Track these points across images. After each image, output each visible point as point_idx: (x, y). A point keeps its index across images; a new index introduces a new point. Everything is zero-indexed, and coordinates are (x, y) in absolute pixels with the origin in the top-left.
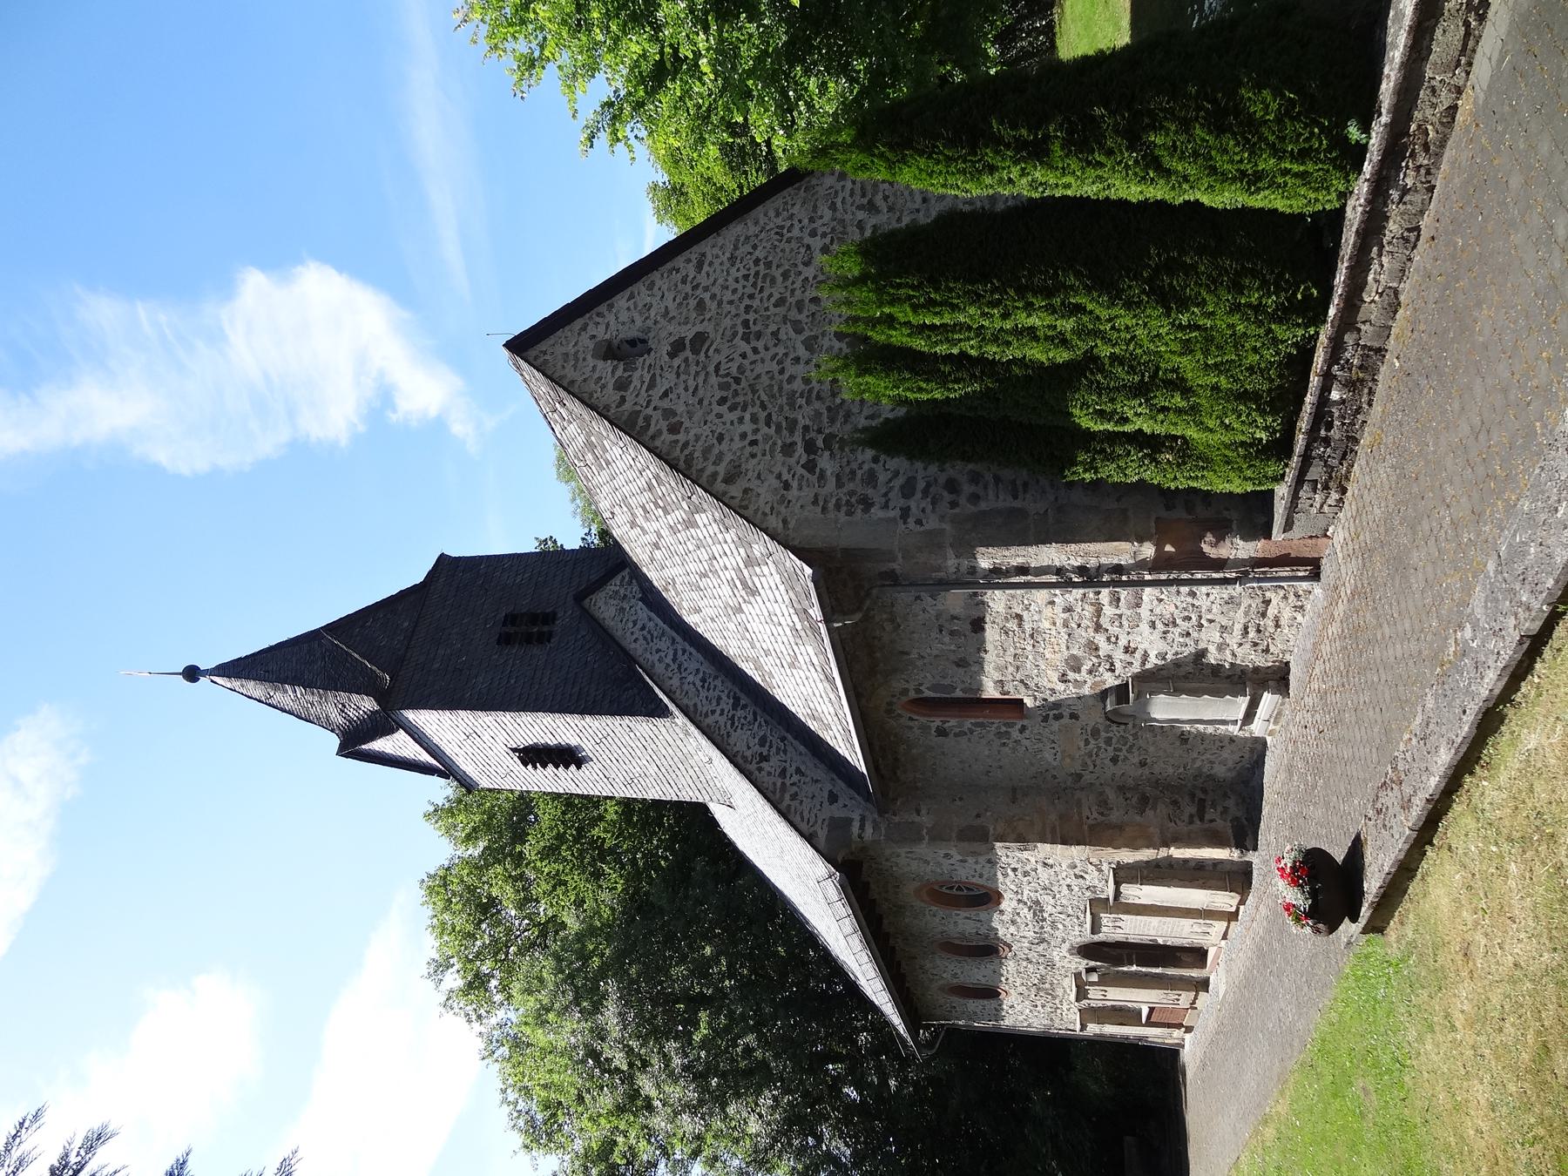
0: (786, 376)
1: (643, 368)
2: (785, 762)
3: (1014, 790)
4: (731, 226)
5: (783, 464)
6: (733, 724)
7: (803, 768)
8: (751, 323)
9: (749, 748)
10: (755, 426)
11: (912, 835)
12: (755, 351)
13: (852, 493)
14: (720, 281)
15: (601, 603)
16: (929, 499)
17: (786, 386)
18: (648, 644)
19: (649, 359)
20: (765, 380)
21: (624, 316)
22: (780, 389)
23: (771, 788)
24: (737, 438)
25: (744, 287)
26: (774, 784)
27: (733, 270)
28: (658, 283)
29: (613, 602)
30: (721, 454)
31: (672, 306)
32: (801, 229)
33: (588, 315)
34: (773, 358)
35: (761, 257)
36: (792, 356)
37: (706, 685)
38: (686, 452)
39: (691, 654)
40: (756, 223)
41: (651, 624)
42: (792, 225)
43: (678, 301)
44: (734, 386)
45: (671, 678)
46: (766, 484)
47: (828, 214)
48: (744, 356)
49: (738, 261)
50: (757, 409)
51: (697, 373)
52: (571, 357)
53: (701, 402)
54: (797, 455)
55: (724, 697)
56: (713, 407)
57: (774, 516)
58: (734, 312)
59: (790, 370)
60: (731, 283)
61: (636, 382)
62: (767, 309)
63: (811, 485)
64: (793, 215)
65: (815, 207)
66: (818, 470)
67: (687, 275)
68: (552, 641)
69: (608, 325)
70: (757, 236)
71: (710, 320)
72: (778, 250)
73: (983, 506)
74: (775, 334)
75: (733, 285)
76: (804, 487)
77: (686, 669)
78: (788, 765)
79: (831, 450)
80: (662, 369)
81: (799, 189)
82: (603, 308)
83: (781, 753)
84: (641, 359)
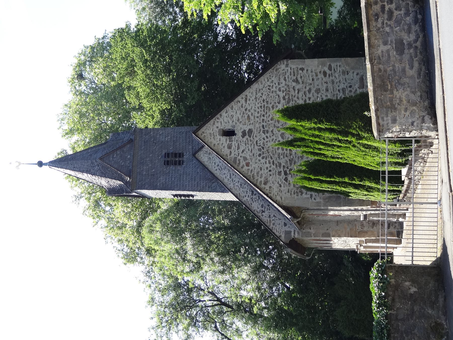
1: (235, 141)
3: (337, 222)
6: (252, 200)
7: (276, 215)
9: (258, 208)
11: (309, 235)
12: (267, 137)
14: (253, 108)
15: (202, 156)
22: (276, 152)
23: (266, 221)
24: (265, 169)
25: (261, 111)
26: (267, 220)
27: (257, 103)
28: (234, 107)
29: (205, 155)
30: (262, 174)
31: (240, 117)
32: (276, 87)
33: (214, 118)
36: (278, 140)
37: (242, 186)
38: (252, 173)
39: (235, 175)
44: (262, 150)
46: (275, 185)
47: (284, 82)
49: (258, 100)
50: (270, 159)
52: (212, 135)
53: (253, 155)
55: (249, 191)
58: (259, 121)
60: (257, 109)
61: (233, 146)
66: (288, 181)
68: (184, 164)
70: (262, 89)
72: (270, 96)
75: (257, 110)
77: (235, 181)
81: (274, 69)
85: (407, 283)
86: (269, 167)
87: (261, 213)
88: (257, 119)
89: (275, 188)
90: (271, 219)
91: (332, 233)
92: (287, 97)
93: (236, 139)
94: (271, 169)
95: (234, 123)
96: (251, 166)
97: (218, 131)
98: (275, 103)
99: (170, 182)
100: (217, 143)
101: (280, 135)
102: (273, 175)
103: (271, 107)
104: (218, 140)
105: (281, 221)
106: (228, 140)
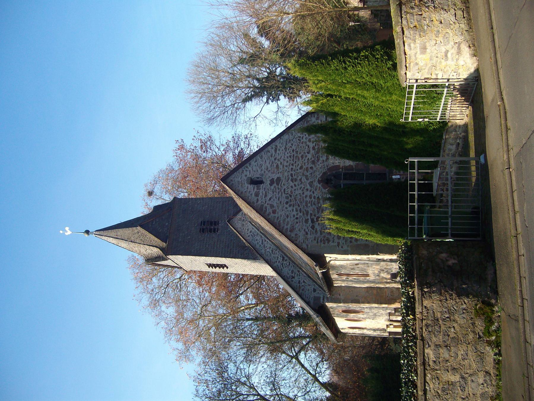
0: (304, 195)
6: (283, 266)
7: (305, 281)
9: (288, 274)
12: (295, 185)
14: (283, 157)
15: (236, 222)
18: (253, 237)
20: (298, 196)
22: (303, 200)
24: (292, 216)
25: (290, 160)
27: (286, 153)
28: (264, 156)
29: (239, 221)
31: (269, 166)
32: (306, 138)
34: (300, 189)
36: (306, 188)
37: (273, 252)
38: (278, 221)
39: (267, 242)
41: (253, 230)
42: (303, 137)
43: (270, 164)
44: (290, 198)
45: (262, 250)
48: (292, 187)
49: (287, 150)
50: (297, 207)
53: (281, 203)
55: (279, 257)
58: (288, 170)
59: (306, 193)
60: (286, 158)
61: (261, 194)
67: (272, 154)
68: (219, 232)
70: (292, 140)
71: (281, 173)
74: (300, 180)
77: (266, 247)
80: (268, 190)
81: (304, 122)
82: (248, 165)
85: (444, 255)
89: (301, 234)
92: (316, 147)
93: (264, 187)
94: (298, 216)
95: (263, 172)
98: (305, 153)
101: (309, 184)
102: (300, 222)
103: (300, 157)
105: (310, 286)
106: (256, 188)
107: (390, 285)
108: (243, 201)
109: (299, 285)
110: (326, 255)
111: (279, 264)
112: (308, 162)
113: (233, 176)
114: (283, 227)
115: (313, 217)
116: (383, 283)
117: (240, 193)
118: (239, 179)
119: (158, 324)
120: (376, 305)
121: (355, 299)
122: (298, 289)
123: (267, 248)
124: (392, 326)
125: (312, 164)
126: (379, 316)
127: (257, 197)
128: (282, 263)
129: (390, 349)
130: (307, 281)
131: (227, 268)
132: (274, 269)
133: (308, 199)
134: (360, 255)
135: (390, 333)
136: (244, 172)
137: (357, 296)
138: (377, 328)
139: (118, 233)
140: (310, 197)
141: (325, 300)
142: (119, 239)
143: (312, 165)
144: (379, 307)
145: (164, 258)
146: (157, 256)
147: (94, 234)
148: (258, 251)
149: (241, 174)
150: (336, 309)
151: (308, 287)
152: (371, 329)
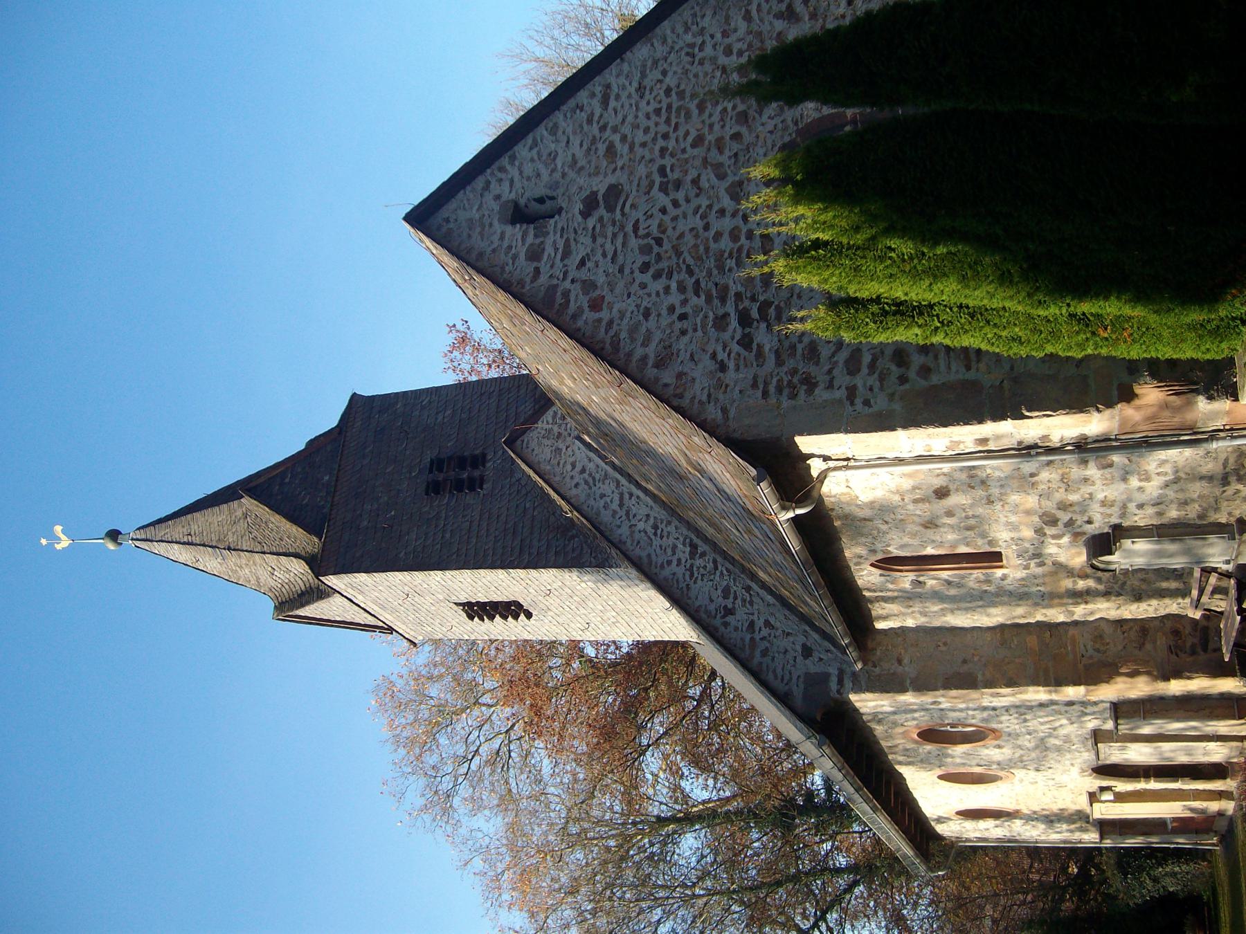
0: (712, 233)
2: (753, 614)
4: (635, 49)
5: (717, 340)
6: (692, 575)
7: (772, 621)
8: (668, 169)
10: (683, 297)
12: (676, 204)
13: (794, 372)
14: (630, 118)
15: (533, 444)
16: (876, 375)
17: (712, 245)
18: (590, 488)
19: (560, 221)
20: (689, 239)
21: (528, 169)
22: (707, 249)
24: (664, 312)
25: (657, 124)
26: (742, 640)
27: (643, 104)
28: (562, 124)
29: (546, 442)
31: (579, 154)
32: (714, 46)
34: (696, 212)
35: (673, 85)
36: (716, 208)
38: (612, 333)
39: (638, 497)
40: (664, 42)
42: (703, 42)
43: (585, 147)
44: (656, 249)
45: (619, 527)
46: (700, 366)
47: (742, 26)
48: (663, 211)
49: (647, 92)
50: (684, 275)
51: (615, 235)
53: (621, 270)
54: (731, 328)
56: (635, 275)
57: (712, 404)
58: (648, 156)
59: (716, 225)
61: (549, 250)
62: (684, 151)
63: (749, 364)
64: (703, 29)
65: (727, 18)
66: (755, 346)
67: (592, 114)
68: (485, 486)
69: (512, 181)
70: (666, 59)
71: (622, 168)
73: (935, 379)
74: (695, 182)
76: (742, 367)
77: (634, 516)
78: (755, 618)
79: (767, 321)
80: (576, 232)
82: (505, 161)
83: (748, 605)
84: (552, 221)
86: (677, 306)
87: (724, 617)
88: (639, 151)
90: (757, 637)
91: (984, 675)
93: (559, 226)
94: (688, 309)
95: (557, 175)
96: (611, 309)
97: (497, 208)
99: (439, 546)
100: (491, 249)
101: (727, 190)
104: (496, 238)
105: (791, 639)
106: (532, 232)
107: (1090, 606)
108: (502, 296)
109: (752, 639)
110: (806, 443)
111: (680, 571)
112: (722, 120)
113: (453, 205)
114: (629, 355)
115: (747, 303)
116: (1060, 596)
117: (474, 256)
118: (474, 211)
119: (466, 865)
120: (1037, 694)
121: (959, 674)
122: (748, 651)
123: (639, 517)
124: (1108, 796)
125: (738, 122)
126: (1059, 749)
127: (535, 264)
128: (688, 566)
129: (1108, 895)
130: (781, 620)
131: (529, 615)
132: (679, 600)
133: (725, 244)
134: (945, 426)
135: (1105, 827)
136: (492, 186)
137: (965, 662)
138: (1055, 808)
139: (194, 528)
140: (734, 236)
141: (848, 684)
142: (196, 545)
143: (736, 129)
144: (1053, 703)
145: (321, 591)
146: (303, 588)
147: (132, 539)
148: (607, 534)
149: (482, 195)
150: (895, 724)
151: (784, 643)
152: (1032, 818)
